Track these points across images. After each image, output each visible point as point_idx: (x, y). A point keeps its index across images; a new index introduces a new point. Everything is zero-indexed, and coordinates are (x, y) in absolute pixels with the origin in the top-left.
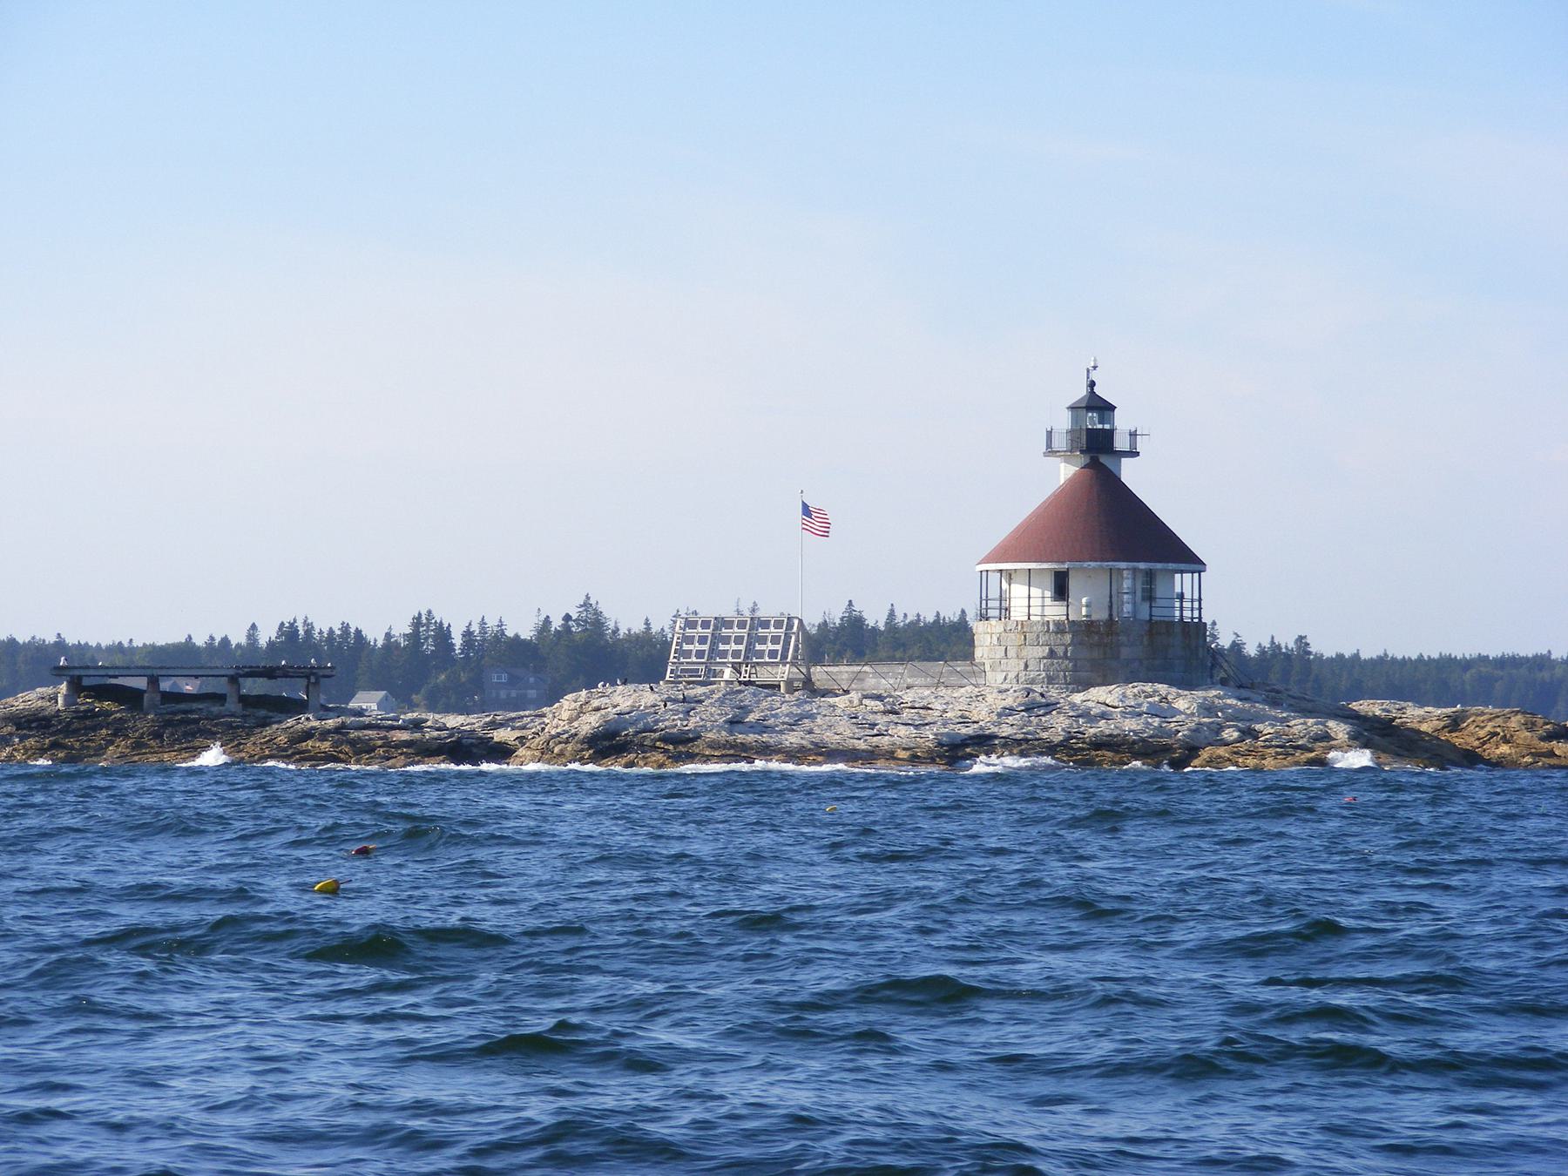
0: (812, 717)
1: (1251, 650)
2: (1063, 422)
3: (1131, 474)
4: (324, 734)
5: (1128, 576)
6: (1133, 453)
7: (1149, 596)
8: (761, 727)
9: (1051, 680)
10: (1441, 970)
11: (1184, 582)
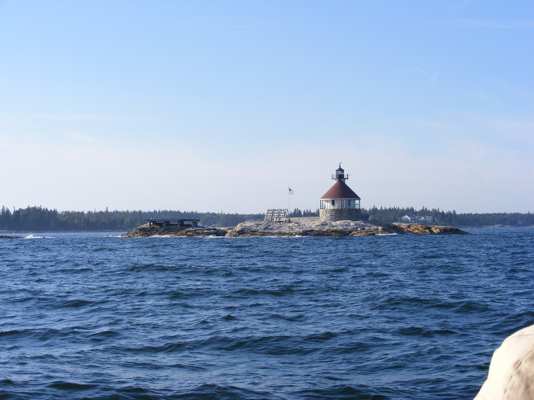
0: (281, 227)
1: (445, 213)
2: (335, 173)
3: (347, 182)
4: (191, 231)
5: (345, 201)
6: (348, 179)
7: (349, 204)
8: (271, 229)
9: (331, 220)
10: (112, 321)
11: (357, 202)
